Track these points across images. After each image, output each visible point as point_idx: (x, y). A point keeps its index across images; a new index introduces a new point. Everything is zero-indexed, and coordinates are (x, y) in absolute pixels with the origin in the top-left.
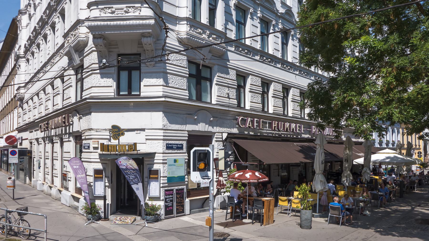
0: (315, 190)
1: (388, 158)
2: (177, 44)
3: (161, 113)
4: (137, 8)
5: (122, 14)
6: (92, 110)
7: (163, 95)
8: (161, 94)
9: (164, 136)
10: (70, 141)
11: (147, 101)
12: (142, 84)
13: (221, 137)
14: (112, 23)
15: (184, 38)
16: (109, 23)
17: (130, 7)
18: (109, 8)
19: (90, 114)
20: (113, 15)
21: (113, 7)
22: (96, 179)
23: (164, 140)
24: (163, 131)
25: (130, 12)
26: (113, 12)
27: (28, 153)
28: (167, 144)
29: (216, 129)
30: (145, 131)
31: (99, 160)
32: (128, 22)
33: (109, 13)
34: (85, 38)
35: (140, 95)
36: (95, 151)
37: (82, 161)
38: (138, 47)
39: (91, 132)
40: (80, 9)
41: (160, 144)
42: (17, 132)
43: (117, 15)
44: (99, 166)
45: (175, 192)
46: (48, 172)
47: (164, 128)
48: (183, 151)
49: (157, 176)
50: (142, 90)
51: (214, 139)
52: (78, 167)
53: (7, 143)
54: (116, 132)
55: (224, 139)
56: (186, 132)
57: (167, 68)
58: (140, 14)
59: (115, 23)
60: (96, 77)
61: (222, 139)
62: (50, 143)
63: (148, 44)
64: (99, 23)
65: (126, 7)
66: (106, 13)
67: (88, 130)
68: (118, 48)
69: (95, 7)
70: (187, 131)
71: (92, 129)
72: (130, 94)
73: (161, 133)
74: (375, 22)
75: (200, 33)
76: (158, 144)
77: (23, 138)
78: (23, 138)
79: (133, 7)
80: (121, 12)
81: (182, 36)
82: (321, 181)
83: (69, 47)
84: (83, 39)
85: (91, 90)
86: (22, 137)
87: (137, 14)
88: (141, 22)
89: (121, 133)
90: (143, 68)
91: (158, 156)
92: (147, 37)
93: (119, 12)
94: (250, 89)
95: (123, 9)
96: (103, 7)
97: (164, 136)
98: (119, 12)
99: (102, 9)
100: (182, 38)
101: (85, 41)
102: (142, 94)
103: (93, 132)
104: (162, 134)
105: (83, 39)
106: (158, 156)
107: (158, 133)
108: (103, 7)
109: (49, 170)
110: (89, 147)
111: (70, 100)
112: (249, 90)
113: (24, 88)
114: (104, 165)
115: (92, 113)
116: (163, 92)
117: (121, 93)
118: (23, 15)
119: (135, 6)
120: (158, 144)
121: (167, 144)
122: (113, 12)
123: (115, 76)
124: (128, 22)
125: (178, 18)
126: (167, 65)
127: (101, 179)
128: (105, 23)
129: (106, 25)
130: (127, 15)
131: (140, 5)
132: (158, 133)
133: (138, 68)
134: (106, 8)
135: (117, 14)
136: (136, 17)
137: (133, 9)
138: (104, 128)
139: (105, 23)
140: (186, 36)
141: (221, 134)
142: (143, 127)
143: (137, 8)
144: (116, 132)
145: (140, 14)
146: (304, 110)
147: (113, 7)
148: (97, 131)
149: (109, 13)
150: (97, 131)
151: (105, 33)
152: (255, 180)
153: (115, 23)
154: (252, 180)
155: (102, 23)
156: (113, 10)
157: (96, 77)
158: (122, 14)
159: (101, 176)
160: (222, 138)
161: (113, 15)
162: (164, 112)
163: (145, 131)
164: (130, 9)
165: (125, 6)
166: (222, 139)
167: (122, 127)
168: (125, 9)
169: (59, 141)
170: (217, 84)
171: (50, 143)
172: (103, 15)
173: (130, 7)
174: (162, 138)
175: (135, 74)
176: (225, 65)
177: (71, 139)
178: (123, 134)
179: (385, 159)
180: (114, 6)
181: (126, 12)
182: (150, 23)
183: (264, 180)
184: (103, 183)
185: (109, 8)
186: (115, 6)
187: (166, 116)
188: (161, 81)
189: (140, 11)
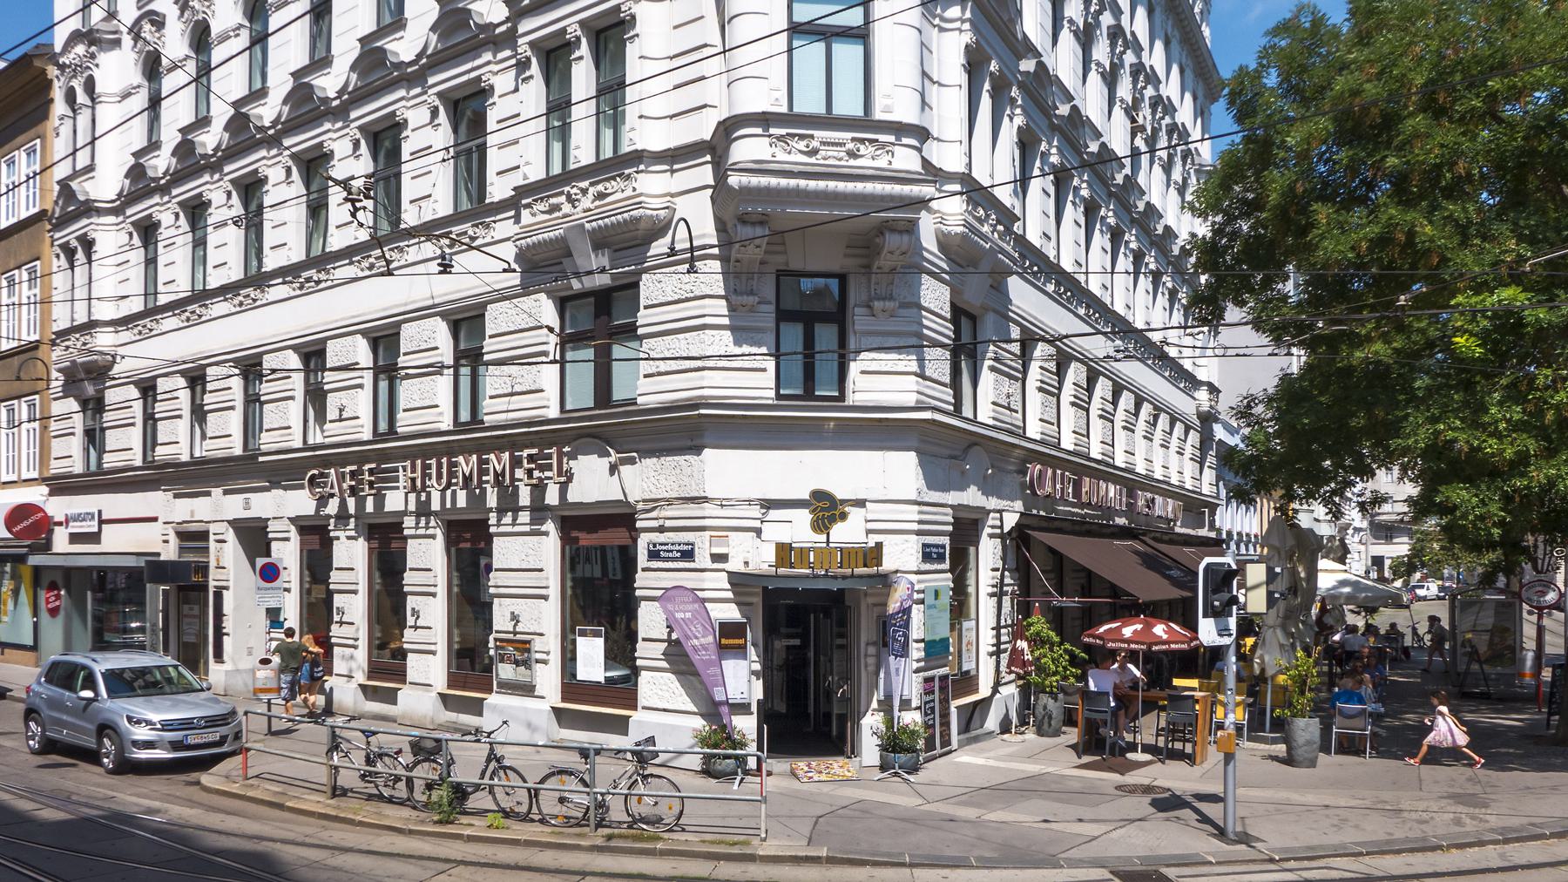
0: (1263, 670)
1: (1343, 583)
2: (936, 250)
3: (913, 454)
4: (883, 145)
5: (840, 159)
6: (706, 441)
7: (918, 402)
8: (911, 400)
9: (920, 522)
10: (546, 534)
11: (880, 420)
12: (854, 368)
13: (998, 523)
14: (812, 184)
15: (956, 234)
16: (802, 183)
17: (862, 141)
19: (697, 450)
20: (813, 160)
22: (724, 650)
23: (919, 533)
24: (916, 508)
25: (862, 156)
26: (814, 152)
27: (197, 572)
28: (924, 545)
29: (993, 503)
30: (864, 506)
31: (730, 595)
32: (859, 187)
33: (801, 152)
34: (662, 212)
35: (842, 397)
36: (716, 566)
37: (704, 600)
38: (846, 256)
39: (703, 508)
40: (641, 117)
41: (909, 545)
42: (45, 490)
43: (822, 162)
44: (732, 613)
45: (937, 680)
46: (356, 640)
47: (919, 499)
48: (940, 567)
50: (850, 386)
51: (987, 530)
52: (688, 615)
53: (10, 531)
54: (823, 509)
55: (1007, 529)
56: (949, 511)
57: (925, 322)
58: (890, 163)
59: (821, 184)
60: (718, 338)
61: (998, 531)
62: (361, 540)
63: (898, 252)
64: (773, 181)
65: (853, 139)
66: (790, 153)
68: (785, 253)
69: (759, 131)
70: (952, 507)
71: (706, 498)
72: (809, 394)
73: (912, 512)
75: (979, 220)
76: (904, 546)
77: (104, 517)
78: (104, 517)
79: (871, 141)
80: (835, 154)
81: (950, 228)
82: (1282, 646)
83: (565, 229)
84: (655, 213)
85: (702, 378)
86: (100, 512)
87: (882, 162)
88: (897, 189)
89: (837, 513)
90: (859, 319)
92: (901, 232)
93: (833, 152)
94: (1042, 382)
96: (783, 131)
97: (920, 522)
98: (830, 153)
99: (780, 138)
100: (949, 233)
101: (660, 221)
102: (852, 399)
103: (709, 509)
104: (917, 517)
105: (655, 213)
107: (903, 512)
108: (783, 131)
109: (358, 630)
110: (688, 555)
111: (543, 399)
112: (1039, 384)
113: (112, 329)
114: (744, 608)
115: (707, 451)
116: (918, 392)
117: (782, 392)
118: (101, 50)
119: (877, 141)
120: (904, 546)
121: (924, 545)
122: (814, 152)
123: (772, 338)
124: (859, 187)
125: (940, 173)
126: (924, 313)
127: (740, 652)
128: (793, 182)
129: (793, 189)
130: (852, 162)
131: (891, 138)
132: (903, 512)
133: (839, 317)
134: (793, 136)
135: (825, 159)
136: (878, 173)
138: (746, 498)
139: (793, 182)
140: (962, 228)
141: (998, 515)
142: (861, 496)
143: (883, 145)
144: (823, 509)
145: (890, 163)
147: (812, 137)
148: (722, 505)
149: (801, 152)
150: (722, 505)
151: (784, 210)
152: (1183, 643)
153: (821, 184)
154: (1176, 643)
155: (784, 182)
156: (815, 144)
157: (718, 338)
158: (840, 159)
159: (741, 641)
160: (1001, 527)
161: (813, 160)
162: (920, 453)
163: (864, 506)
164: (862, 147)
165: (849, 135)
166: (998, 531)
167: (840, 495)
168: (850, 146)
169: (439, 532)
170: (992, 369)
171: (361, 540)
172: (782, 156)
173: (862, 141)
174: (915, 526)
175: (826, 336)
176: (1002, 310)
177: (550, 526)
178: (843, 516)
179: (1334, 588)
180: (816, 133)
181: (852, 155)
182: (922, 194)
183: (1173, 646)
184: (743, 664)
185: (802, 137)
187: (922, 464)
188: (909, 363)
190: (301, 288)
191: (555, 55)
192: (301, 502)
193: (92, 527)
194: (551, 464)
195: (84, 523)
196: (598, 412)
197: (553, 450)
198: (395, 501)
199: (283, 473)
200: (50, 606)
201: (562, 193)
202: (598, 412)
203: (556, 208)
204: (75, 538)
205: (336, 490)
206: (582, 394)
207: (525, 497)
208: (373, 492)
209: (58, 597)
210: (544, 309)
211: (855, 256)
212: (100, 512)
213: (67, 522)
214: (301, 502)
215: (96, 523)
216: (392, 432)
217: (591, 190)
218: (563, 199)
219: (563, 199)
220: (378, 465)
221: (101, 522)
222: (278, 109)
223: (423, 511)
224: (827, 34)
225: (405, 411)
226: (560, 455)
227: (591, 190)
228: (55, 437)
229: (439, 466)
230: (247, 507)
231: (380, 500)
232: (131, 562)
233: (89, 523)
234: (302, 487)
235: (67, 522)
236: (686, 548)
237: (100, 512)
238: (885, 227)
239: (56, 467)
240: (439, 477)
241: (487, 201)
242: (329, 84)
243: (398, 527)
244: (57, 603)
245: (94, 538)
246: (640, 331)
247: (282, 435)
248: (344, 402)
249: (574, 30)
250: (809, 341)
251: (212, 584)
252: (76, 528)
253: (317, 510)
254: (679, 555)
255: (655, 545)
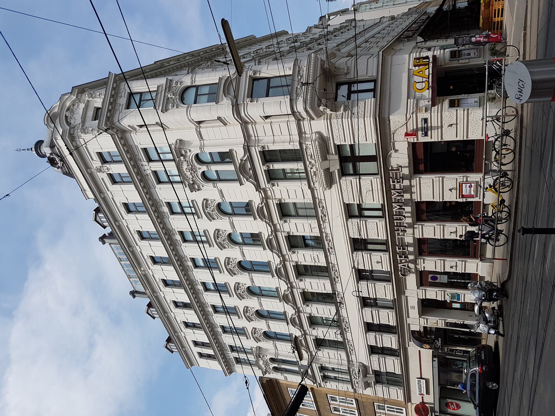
17: (319, 206)
18: (322, 217)
21: (321, 216)
49: (456, 101)
58: (310, 145)
65: (320, 208)
67: (336, 370)
74: (552, 100)
77: (419, 377)
78: (419, 377)
91: (367, 268)
95: (328, 243)
106: (367, 268)
134: (312, 181)
137: (308, 150)
145: (310, 145)
146: (450, 215)
156: (323, 215)
165: (319, 209)
173: (319, 206)
180: (327, 248)
186: (327, 247)
189: (308, 144)
190: (348, 328)
191: (272, 176)
192: (411, 280)
193: (423, 382)
194: (398, 211)
195: (422, 386)
196: (378, 160)
197: (395, 221)
198: (409, 239)
199: (400, 289)
200: (456, 408)
201: (310, 171)
202: (378, 160)
203: (315, 173)
204: (428, 393)
205: (406, 264)
206: (371, 167)
207: (406, 183)
208: (406, 248)
209: (452, 403)
210: (346, 182)
211: (331, 78)
212: (417, 378)
213: (422, 395)
214: (411, 280)
215: (422, 380)
216: (385, 243)
217: (310, 160)
218: (312, 170)
219: (312, 170)
220: (397, 245)
221: (421, 378)
222: (296, 329)
223: (415, 262)
224: (269, 87)
225: (378, 237)
226: (392, 170)
227: (310, 160)
228: (390, 397)
229: (397, 220)
230: (413, 308)
231: (409, 245)
232: (436, 364)
233: (422, 384)
234: (405, 279)
235: (422, 395)
236: (423, 122)
237: (417, 378)
238: (322, 68)
239: (401, 398)
240: (400, 219)
241: (320, 236)
242: (290, 311)
243: (420, 240)
244: (454, 404)
245: (427, 381)
246: (352, 143)
247: (388, 290)
248: (376, 261)
249: (265, 168)
250: (355, 92)
251: (443, 327)
252: (424, 391)
253: (413, 273)
254: (426, 124)
255: (423, 134)
